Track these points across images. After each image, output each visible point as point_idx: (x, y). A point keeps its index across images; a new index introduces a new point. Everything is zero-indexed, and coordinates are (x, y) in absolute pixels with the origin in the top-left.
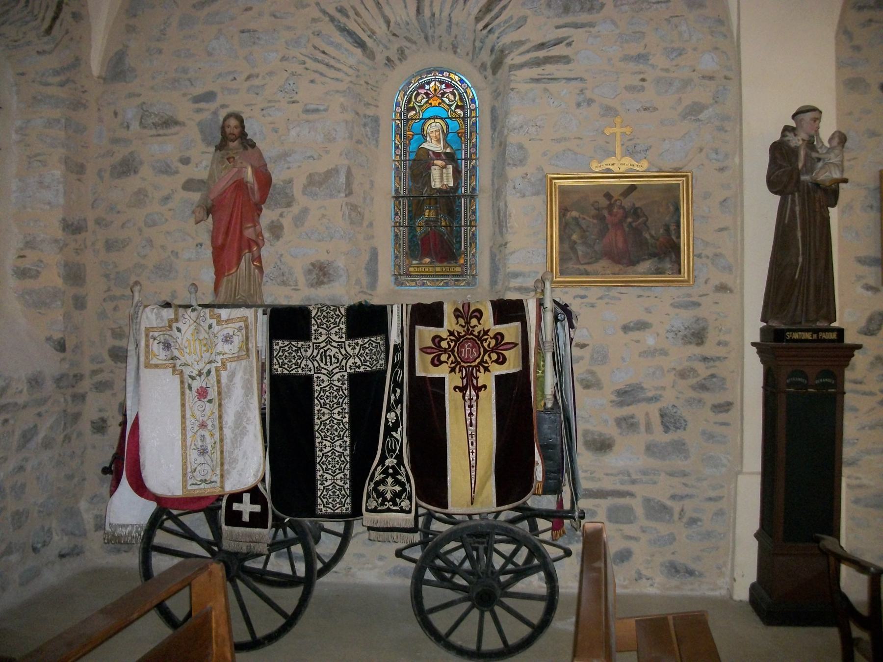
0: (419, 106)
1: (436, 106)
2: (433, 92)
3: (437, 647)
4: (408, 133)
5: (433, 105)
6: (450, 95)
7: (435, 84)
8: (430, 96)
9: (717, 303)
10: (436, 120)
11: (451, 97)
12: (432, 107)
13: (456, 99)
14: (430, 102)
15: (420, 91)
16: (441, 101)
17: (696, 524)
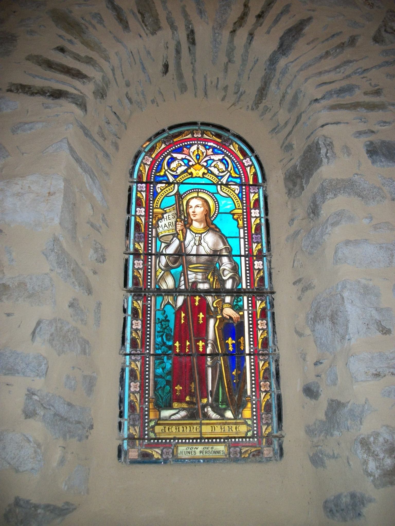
0: (174, 176)
1: (199, 177)
2: (194, 158)
3: (135, 152)
4: (155, 210)
5: (194, 176)
6: (219, 163)
7: (198, 149)
8: (191, 164)
9: (318, 376)
10: (201, 195)
11: (222, 166)
12: (192, 177)
13: (229, 169)
14: (189, 171)
15: (175, 155)
16: (206, 171)
17: (95, 253)
